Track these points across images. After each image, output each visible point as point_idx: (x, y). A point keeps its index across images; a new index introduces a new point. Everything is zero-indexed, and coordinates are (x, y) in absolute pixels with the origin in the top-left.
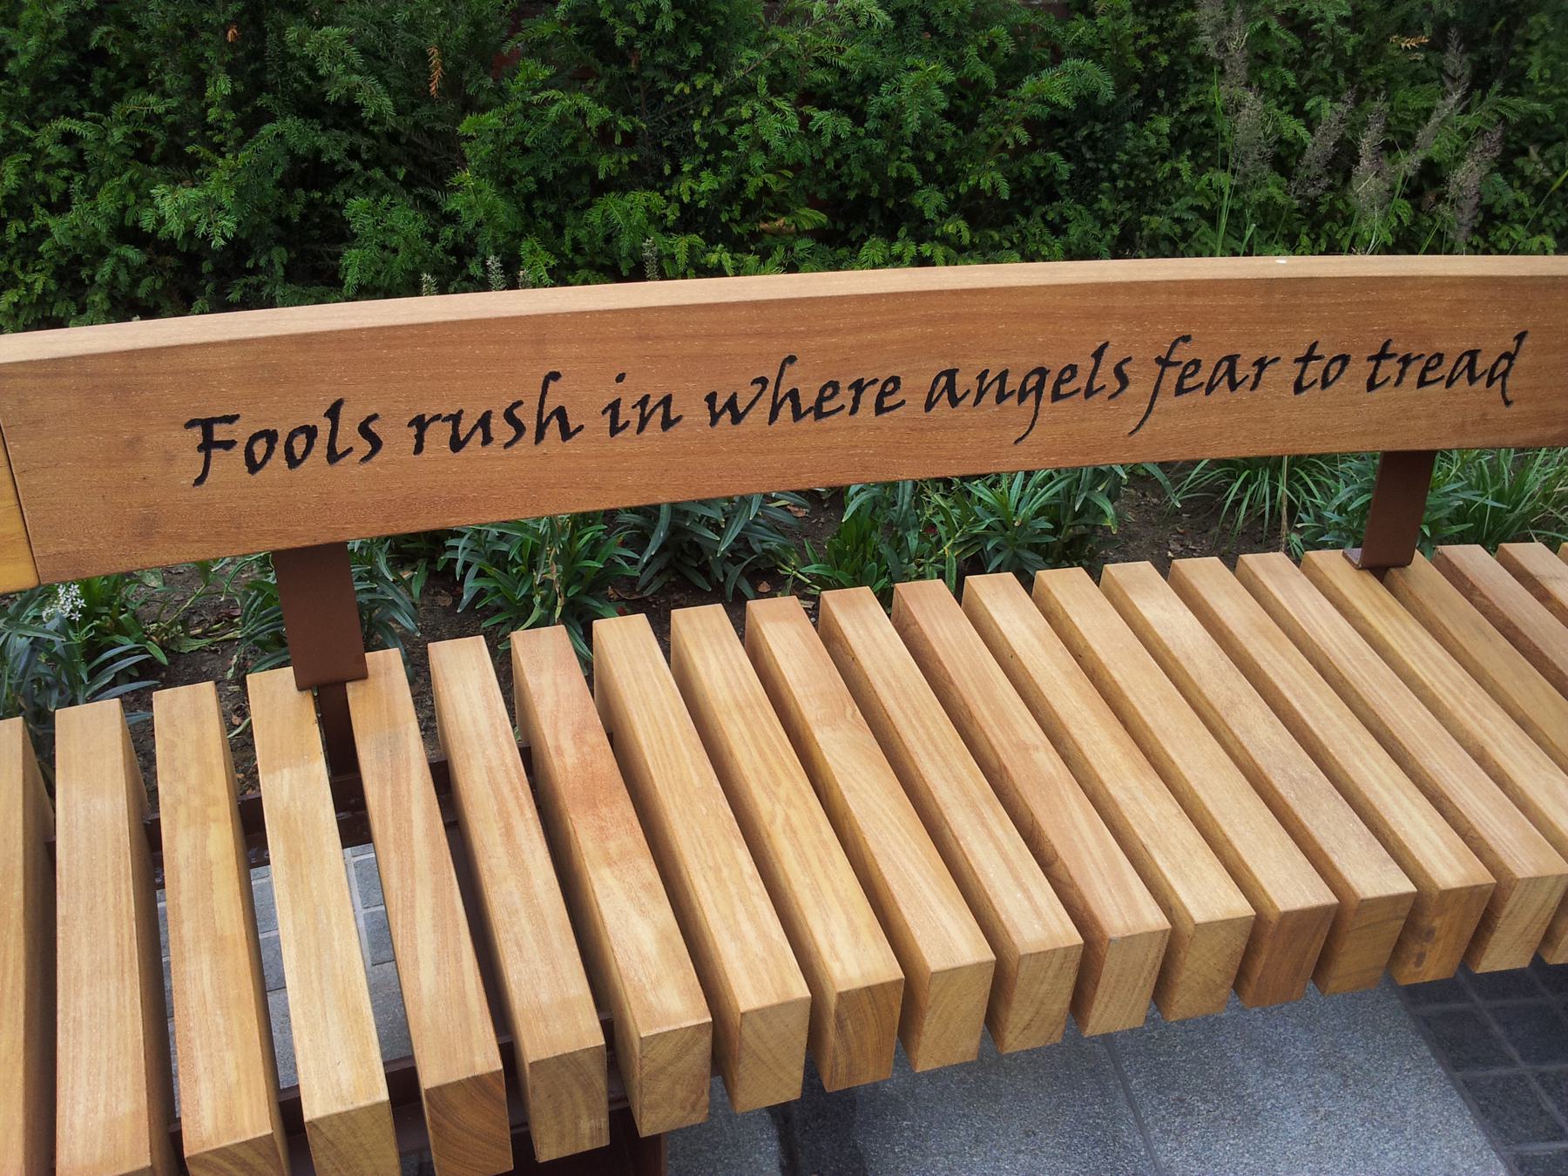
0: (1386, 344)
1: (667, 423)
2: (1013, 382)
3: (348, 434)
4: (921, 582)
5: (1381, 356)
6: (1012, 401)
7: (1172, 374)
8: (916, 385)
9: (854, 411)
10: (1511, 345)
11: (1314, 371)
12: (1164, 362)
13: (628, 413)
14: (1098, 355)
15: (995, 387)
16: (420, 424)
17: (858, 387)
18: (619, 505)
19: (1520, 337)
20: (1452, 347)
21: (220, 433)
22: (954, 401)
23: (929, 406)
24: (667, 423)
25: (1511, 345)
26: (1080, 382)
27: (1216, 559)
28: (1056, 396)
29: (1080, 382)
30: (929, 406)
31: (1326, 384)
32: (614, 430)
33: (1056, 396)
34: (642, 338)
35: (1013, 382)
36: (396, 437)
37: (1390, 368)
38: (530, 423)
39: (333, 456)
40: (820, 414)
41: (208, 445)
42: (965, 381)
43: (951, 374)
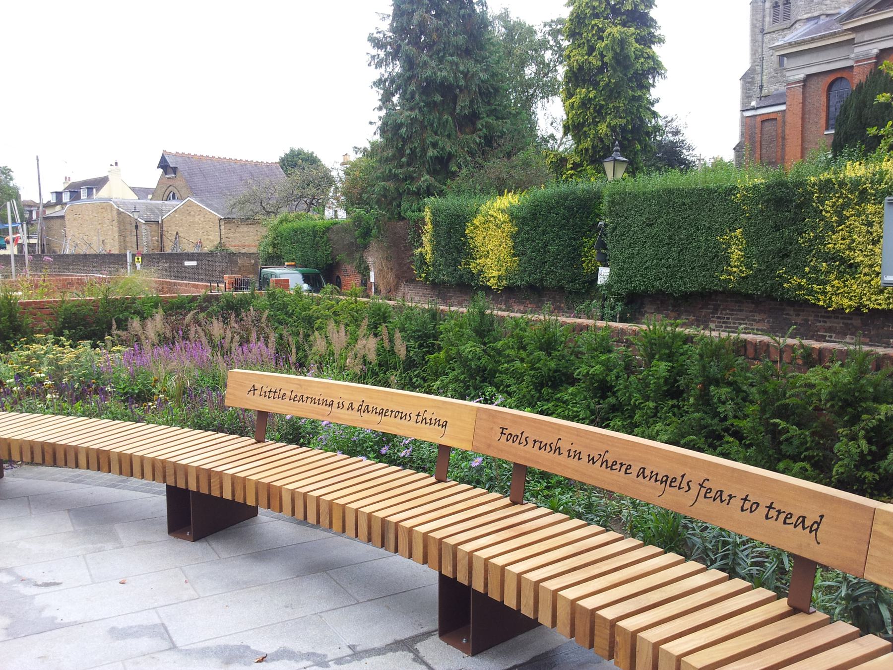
0: (772, 503)
1: (579, 459)
2: (659, 478)
3: (267, 394)
4: (292, 449)
5: (770, 507)
6: (659, 483)
7: (703, 490)
8: (346, 405)
9: (776, 520)
10: (818, 520)
11: (747, 505)
12: (701, 486)
13: (572, 454)
14: (683, 476)
15: (654, 476)
16: (535, 441)
17: (622, 464)
18: (819, 561)
19: (822, 517)
20: (797, 513)
21: (505, 431)
22: (644, 478)
23: (638, 476)
24: (579, 459)
25: (818, 520)
26: (677, 484)
27: (737, 579)
28: (671, 486)
29: (677, 484)
30: (638, 476)
31: (751, 511)
32: (569, 456)
33: (671, 486)
34: (578, 435)
35: (659, 478)
36: (531, 443)
37: (773, 513)
38: (548, 446)
39: (520, 443)
40: (612, 469)
41: (502, 433)
42: (647, 473)
43: (644, 469)
